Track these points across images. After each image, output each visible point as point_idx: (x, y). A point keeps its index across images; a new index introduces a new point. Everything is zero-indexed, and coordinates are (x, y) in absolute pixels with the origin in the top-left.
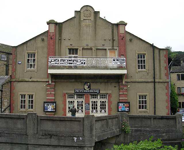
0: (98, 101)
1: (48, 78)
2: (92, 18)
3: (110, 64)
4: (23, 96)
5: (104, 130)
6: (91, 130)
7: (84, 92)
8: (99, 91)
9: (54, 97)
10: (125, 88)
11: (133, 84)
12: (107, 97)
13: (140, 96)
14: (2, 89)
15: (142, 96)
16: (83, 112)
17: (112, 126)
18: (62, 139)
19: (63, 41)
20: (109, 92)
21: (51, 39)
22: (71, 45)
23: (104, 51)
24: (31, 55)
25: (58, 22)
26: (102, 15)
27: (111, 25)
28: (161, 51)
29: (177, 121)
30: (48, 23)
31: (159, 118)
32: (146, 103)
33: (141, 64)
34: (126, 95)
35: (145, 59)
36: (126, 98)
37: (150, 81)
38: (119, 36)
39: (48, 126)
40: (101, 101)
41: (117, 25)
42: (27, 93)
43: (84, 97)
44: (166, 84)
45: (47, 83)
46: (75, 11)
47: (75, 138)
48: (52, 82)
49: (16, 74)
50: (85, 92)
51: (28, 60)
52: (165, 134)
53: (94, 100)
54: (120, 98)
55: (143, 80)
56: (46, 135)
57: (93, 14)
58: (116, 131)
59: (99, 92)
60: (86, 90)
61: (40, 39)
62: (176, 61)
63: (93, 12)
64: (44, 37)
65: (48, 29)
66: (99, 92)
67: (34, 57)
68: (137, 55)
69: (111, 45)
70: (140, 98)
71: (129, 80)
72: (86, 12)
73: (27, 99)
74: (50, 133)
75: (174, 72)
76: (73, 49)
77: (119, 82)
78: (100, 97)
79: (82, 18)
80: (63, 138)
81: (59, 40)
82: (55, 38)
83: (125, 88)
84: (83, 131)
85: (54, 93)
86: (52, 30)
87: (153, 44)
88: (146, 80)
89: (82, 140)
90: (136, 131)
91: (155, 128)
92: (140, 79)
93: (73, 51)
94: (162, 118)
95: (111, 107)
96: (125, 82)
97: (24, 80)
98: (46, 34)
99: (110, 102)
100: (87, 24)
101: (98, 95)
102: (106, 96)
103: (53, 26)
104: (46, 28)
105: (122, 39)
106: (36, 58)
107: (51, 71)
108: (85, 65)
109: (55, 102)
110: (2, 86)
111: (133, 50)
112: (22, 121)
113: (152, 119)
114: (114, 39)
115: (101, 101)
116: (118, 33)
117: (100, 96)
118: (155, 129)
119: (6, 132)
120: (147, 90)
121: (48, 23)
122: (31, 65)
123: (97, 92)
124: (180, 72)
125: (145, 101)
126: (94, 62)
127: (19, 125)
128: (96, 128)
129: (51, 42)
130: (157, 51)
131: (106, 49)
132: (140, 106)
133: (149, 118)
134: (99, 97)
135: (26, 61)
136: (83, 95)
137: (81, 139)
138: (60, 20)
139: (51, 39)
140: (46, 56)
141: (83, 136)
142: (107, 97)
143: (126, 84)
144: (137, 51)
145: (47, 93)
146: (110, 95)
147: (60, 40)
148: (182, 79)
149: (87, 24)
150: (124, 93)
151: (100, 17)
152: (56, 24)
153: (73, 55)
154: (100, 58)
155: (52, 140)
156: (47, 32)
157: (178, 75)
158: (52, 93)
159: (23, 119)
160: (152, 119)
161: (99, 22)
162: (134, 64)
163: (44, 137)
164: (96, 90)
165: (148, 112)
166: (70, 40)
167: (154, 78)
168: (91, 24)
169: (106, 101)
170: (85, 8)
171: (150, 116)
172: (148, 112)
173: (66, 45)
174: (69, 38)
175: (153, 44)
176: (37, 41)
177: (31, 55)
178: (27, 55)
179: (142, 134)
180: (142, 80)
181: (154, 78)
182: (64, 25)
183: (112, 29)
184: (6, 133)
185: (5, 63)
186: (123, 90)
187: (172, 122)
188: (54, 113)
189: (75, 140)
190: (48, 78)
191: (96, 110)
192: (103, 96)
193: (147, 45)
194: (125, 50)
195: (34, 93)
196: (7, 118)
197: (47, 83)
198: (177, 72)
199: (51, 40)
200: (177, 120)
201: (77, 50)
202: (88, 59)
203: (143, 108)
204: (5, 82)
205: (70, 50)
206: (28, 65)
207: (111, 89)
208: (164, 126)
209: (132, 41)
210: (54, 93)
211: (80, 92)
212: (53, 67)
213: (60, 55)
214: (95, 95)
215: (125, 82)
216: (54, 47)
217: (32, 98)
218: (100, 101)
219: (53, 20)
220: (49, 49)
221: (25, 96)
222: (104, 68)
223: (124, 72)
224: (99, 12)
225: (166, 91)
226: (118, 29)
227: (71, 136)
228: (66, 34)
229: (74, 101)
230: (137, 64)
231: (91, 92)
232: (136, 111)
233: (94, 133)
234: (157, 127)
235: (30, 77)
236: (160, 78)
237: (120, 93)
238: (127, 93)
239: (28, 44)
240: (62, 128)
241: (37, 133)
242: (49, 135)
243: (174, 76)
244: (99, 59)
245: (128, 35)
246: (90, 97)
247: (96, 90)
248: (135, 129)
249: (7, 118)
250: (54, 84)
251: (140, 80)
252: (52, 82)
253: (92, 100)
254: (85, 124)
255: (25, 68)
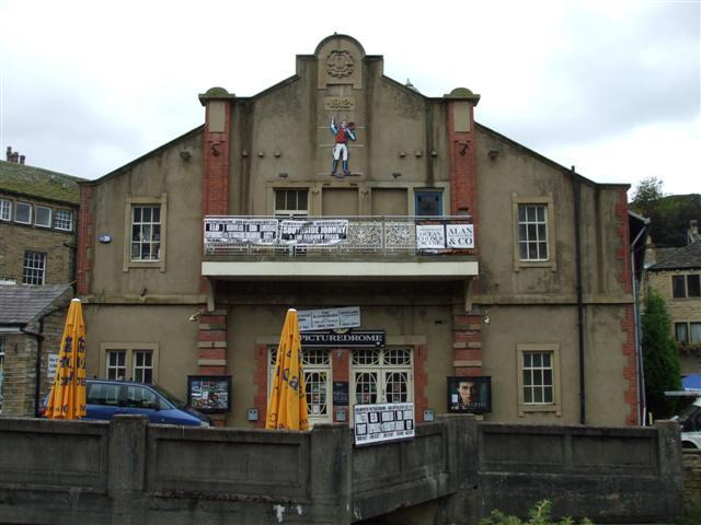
0: (378, 371)
1: (202, 290)
2: (357, 80)
3: (434, 245)
4: (117, 356)
5: (388, 479)
6: (337, 478)
7: (329, 342)
8: (383, 338)
9: (226, 358)
10: (473, 327)
11: (503, 313)
12: (412, 360)
13: (527, 355)
14: (41, 331)
15: (537, 355)
16: (324, 412)
17: (422, 465)
18: (232, 512)
19: (255, 159)
20: (419, 340)
21: (216, 154)
22: (285, 176)
23: (398, 197)
24: (147, 212)
25: (237, 96)
26: (391, 70)
27: (423, 105)
28: (604, 195)
29: (663, 450)
30: (206, 100)
31: (592, 437)
32: (548, 379)
33: (532, 240)
34: (477, 353)
35: (546, 222)
36: (479, 363)
37: (561, 299)
38: (451, 146)
39: (183, 465)
40: (388, 374)
41: (445, 103)
42: (129, 347)
43: (330, 360)
44: (622, 312)
45: (202, 311)
46: (300, 58)
47: (280, 509)
48: (216, 308)
49: (92, 278)
50: (333, 342)
51: (136, 229)
52: (615, 496)
53: (367, 371)
54: (457, 363)
55: (539, 298)
56: (175, 496)
57: (359, 66)
58: (435, 482)
59: (383, 342)
60: (336, 334)
61: (175, 154)
62: (659, 223)
63: (359, 58)
64: (189, 150)
65: (202, 122)
66: (383, 342)
67: (157, 218)
68: (516, 207)
69: (423, 175)
70: (527, 364)
71: (485, 299)
72: (335, 60)
73: (131, 364)
74: (191, 488)
75: (661, 270)
76: (292, 191)
77: (451, 307)
78: (387, 360)
79: (324, 79)
80: (236, 507)
81: (242, 161)
82: (227, 150)
83: (473, 327)
84: (309, 480)
85: (223, 344)
86: (219, 124)
87: (573, 167)
88: (551, 299)
89: (304, 514)
90: (512, 481)
91: (579, 473)
92: (527, 293)
93: (291, 197)
94: (606, 435)
95: (426, 394)
96: (473, 305)
97: (157, 299)
98: (199, 138)
99: (420, 379)
100: (344, 97)
101: (378, 351)
102: (407, 355)
103: (220, 111)
104: (195, 117)
105: (463, 153)
106: (162, 222)
107: (211, 269)
108: (328, 243)
109: (228, 379)
110: (41, 321)
111: (502, 189)
112: (92, 445)
113: (568, 438)
114: (434, 153)
115: (388, 374)
116: (447, 129)
117: (387, 355)
118: (581, 476)
119: (33, 486)
120: (554, 333)
121: (206, 100)
122: (146, 247)
123: (374, 343)
124: (686, 269)
125: (548, 374)
126: (362, 236)
127: (83, 461)
128: (356, 470)
129: (216, 165)
130: (586, 193)
131: (406, 189)
132: (527, 392)
133: (557, 434)
134: (381, 358)
135: (129, 232)
136: (327, 351)
137: (300, 512)
138: (244, 88)
139: (216, 154)
140: (195, 213)
141: (309, 501)
142: (412, 360)
143: (477, 311)
144: (515, 194)
145: (201, 344)
146: (421, 353)
147: (245, 161)
148: (694, 292)
149: (344, 97)
150: (471, 345)
151: (386, 74)
152: (233, 102)
153: (291, 212)
154: (382, 219)
155: (200, 513)
156: (199, 132)
157: (678, 281)
158: (218, 344)
159: (98, 437)
160: (568, 438)
161: (383, 97)
162: (505, 236)
163: (169, 504)
164: (370, 335)
165: (558, 413)
166: (280, 160)
167: (579, 290)
168: (351, 100)
169: (405, 374)
170: (332, 46)
171: (559, 428)
172: (558, 413)
173: (266, 175)
174: (279, 151)
175: (573, 167)
176: (164, 164)
177: (147, 212)
178: (129, 212)
179: (531, 495)
180: (533, 296)
181: (579, 290)
182: (258, 105)
183: (427, 119)
184: (36, 492)
185: (70, 240)
186: (468, 333)
187: (641, 452)
188: (223, 417)
189: (279, 515)
190: (202, 290)
191: (322, 406)
192: (396, 355)
193: (543, 173)
194: (474, 188)
195: (554, 347)
196: (40, 434)
197: (202, 311)
198: (674, 269)
199: (214, 158)
200: (662, 443)
201: (304, 192)
202: (386, 224)
203: (538, 399)
204: (51, 307)
205: (279, 192)
206: (136, 247)
207: (427, 334)
208: (613, 465)
209: (498, 158)
210: (223, 344)
211: (316, 343)
212: (223, 254)
213: (245, 208)
214: (369, 354)
215: (473, 305)
216: (226, 183)
217: (148, 363)
218: (384, 372)
219: (222, 91)
220: (206, 190)
221: (122, 354)
222: (395, 257)
223: (470, 268)
224: (379, 58)
225: (623, 337)
226: (447, 118)
227: (265, 501)
228: (269, 134)
229: (375, 374)
230: (517, 240)
231: (355, 342)
232: (513, 409)
233: (348, 490)
234: (587, 470)
235: (140, 289)
236: (601, 291)
237: (459, 345)
238: (479, 345)
239: (136, 171)
240: (234, 473)
241: (144, 490)
242: (188, 495)
243: (662, 284)
244: (381, 224)
245: (482, 138)
246: (351, 360)
247: (370, 335)
248: (508, 477)
249: (40, 434)
250: (224, 312)
251: (526, 298)
252: (217, 305)
253: (356, 369)
254: (315, 459)
255: (126, 257)
